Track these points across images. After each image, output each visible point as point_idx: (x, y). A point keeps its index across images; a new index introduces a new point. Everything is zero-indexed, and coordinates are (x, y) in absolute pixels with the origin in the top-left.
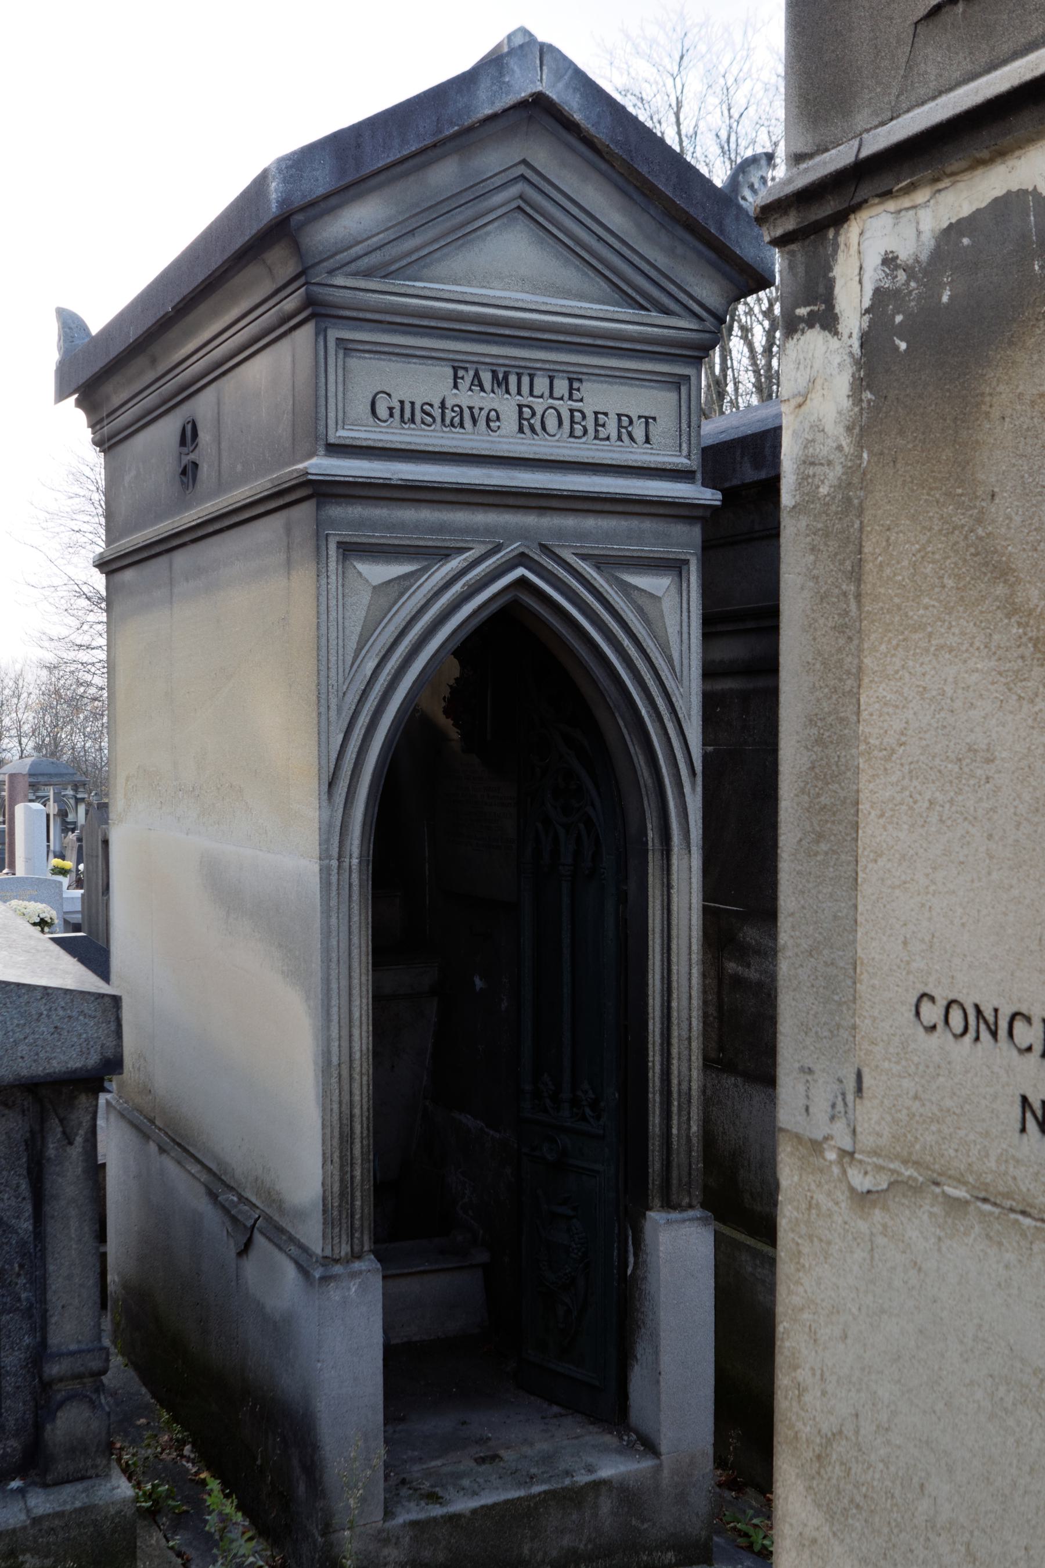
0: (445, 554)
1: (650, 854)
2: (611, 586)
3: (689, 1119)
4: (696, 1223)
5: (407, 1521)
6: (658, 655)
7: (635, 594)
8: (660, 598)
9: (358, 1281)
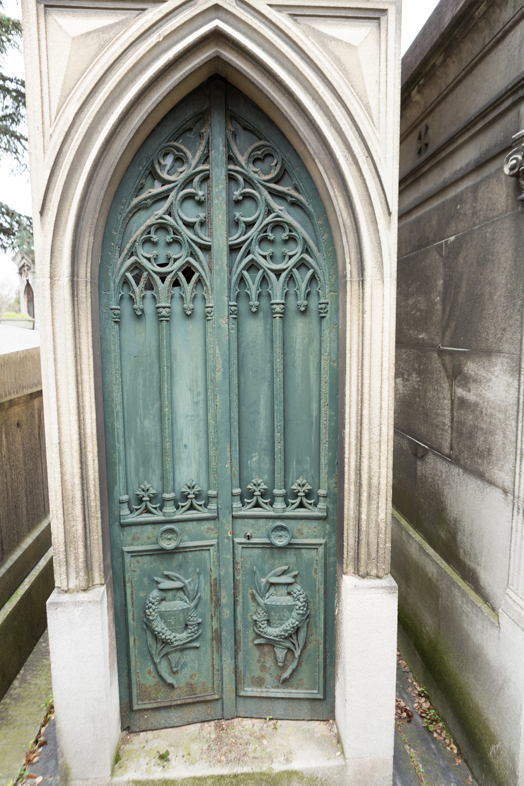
3: (378, 508)
4: (381, 591)
5: (131, 779)
6: (353, 101)
7: (332, 45)
8: (356, 47)
9: (80, 608)
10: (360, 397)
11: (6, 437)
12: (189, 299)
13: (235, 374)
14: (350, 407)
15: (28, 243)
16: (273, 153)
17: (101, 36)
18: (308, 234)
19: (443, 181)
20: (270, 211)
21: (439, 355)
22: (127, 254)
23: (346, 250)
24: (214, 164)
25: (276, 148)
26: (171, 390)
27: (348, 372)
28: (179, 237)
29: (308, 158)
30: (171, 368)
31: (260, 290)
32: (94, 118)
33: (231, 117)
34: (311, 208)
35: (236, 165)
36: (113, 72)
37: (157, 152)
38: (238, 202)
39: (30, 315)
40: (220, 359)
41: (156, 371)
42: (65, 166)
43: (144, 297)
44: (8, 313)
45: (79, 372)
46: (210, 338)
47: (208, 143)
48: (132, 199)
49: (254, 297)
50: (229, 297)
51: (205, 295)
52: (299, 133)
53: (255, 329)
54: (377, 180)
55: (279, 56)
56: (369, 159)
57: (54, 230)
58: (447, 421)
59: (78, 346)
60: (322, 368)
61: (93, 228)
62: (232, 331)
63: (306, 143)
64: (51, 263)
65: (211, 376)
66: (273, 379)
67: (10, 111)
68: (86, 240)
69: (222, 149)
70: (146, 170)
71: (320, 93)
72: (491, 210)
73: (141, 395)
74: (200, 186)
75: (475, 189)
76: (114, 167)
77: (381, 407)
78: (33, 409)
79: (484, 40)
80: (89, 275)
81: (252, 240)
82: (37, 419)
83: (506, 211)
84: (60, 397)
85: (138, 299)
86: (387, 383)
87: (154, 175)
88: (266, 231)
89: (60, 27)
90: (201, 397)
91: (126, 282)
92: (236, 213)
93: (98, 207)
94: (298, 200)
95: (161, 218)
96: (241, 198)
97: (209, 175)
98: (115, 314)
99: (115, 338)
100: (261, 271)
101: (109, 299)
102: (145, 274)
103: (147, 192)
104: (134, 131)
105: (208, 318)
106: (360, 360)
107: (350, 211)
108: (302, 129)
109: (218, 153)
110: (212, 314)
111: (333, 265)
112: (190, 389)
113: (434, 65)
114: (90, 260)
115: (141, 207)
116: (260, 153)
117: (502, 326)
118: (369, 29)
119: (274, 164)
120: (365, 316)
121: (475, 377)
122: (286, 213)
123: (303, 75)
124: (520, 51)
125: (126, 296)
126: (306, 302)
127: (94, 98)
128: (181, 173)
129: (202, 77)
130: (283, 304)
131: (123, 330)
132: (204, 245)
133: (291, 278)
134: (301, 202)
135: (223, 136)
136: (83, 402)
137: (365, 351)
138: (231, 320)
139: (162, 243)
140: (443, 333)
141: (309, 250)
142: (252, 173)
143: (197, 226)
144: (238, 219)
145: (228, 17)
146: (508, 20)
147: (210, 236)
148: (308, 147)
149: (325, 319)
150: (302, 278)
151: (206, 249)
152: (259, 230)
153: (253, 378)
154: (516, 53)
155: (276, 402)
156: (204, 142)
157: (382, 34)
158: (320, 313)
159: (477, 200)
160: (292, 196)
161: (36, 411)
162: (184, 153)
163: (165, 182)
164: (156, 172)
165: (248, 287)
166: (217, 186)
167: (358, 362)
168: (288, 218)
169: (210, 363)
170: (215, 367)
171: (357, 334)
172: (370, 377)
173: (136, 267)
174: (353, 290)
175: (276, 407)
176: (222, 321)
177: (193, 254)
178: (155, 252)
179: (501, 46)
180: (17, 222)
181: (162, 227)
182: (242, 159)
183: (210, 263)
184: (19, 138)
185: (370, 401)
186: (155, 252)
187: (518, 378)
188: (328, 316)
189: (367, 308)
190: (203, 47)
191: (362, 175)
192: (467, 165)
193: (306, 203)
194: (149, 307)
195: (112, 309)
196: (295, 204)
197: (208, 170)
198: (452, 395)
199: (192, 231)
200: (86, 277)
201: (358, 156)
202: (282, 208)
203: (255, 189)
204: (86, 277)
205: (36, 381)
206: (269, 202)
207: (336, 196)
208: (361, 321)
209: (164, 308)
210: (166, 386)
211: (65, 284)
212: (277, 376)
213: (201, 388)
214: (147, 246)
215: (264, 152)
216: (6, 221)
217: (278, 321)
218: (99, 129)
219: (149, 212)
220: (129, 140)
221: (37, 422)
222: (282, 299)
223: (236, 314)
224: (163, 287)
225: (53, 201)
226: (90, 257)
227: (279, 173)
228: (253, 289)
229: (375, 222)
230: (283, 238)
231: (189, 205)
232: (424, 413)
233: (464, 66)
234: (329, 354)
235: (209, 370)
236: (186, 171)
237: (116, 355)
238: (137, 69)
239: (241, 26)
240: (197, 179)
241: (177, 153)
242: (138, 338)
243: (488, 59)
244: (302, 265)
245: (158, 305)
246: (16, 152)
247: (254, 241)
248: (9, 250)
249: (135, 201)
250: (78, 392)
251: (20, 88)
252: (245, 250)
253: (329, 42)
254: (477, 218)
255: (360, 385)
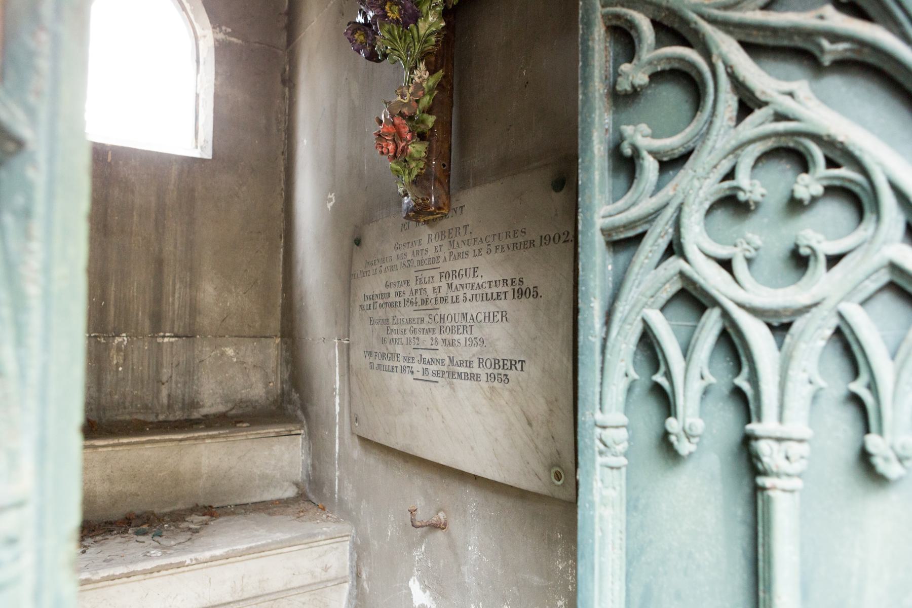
203: (686, 43)
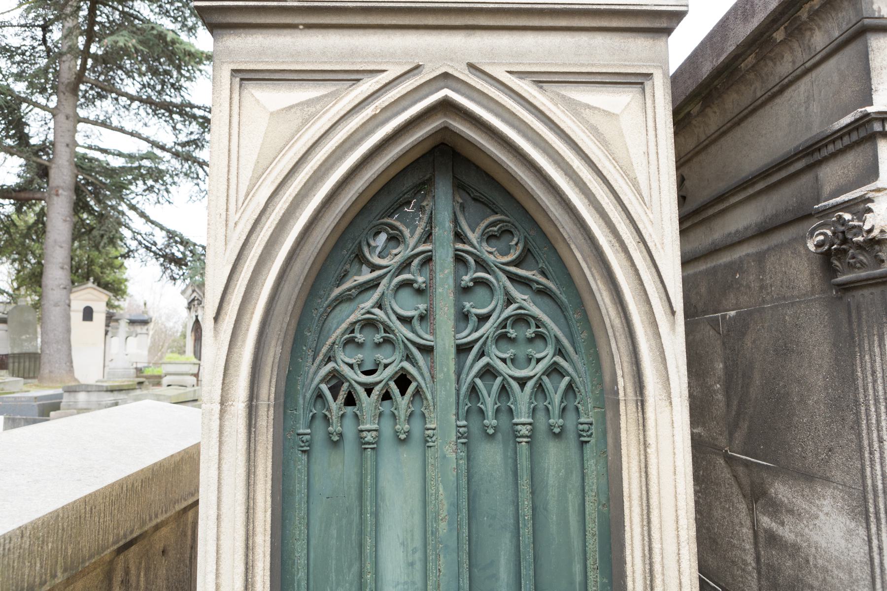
0: (353, 77)
1: (622, 405)
2: (556, 105)
6: (617, 176)
7: (587, 113)
8: (617, 115)
10: (648, 567)
11: (145, 575)
12: (403, 418)
13: (465, 522)
14: (634, 581)
15: (201, 274)
16: (512, 230)
17: (306, 109)
18: (561, 329)
19: (713, 243)
20: (510, 301)
21: (726, 462)
22: (323, 360)
23: (617, 359)
24: (437, 244)
25: (517, 224)
26: (376, 546)
27: (627, 528)
28: (391, 336)
29: (560, 240)
30: (376, 515)
31: (499, 404)
32: (292, 203)
33: (459, 186)
34: (563, 298)
35: (464, 243)
36: (317, 149)
37: (365, 232)
38: (466, 290)
39: (196, 357)
40: (445, 502)
41: (356, 518)
42: (251, 260)
43: (343, 416)
44: (171, 355)
45: (251, 533)
46: (430, 473)
47: (431, 218)
48: (331, 290)
49: (490, 414)
50: (457, 414)
51: (426, 412)
52: (549, 213)
53: (492, 457)
54: (654, 270)
55: (522, 127)
56: (641, 245)
57: (231, 341)
58: (750, 559)
59: (251, 496)
60: (587, 513)
61: (282, 335)
62: (461, 462)
63: (558, 225)
64: (223, 383)
65: (432, 527)
66: (518, 529)
67: (193, 137)
68: (272, 350)
69: (449, 225)
70: (352, 253)
71: (575, 167)
72: (788, 287)
73: (333, 553)
74: (420, 270)
75: (760, 258)
76: (312, 259)
77: (680, 583)
78: (186, 525)
79: (755, 92)
80: (272, 396)
81: (487, 338)
82: (189, 537)
83: (813, 293)
84: (221, 571)
85: (334, 419)
86: (687, 548)
87: (361, 259)
88: (505, 327)
89: (258, 101)
90: (418, 555)
91: (320, 396)
92: (465, 303)
93: (290, 308)
94: (546, 287)
95: (369, 312)
96: (471, 284)
97: (431, 256)
98: (303, 442)
99: (301, 473)
100: (499, 380)
101: (296, 419)
102: (346, 385)
103: (352, 280)
104: (341, 215)
105: (428, 444)
106: (645, 512)
107: (620, 309)
108: (552, 209)
109: (444, 230)
110: (434, 439)
111: (597, 372)
112: (403, 544)
113: (689, 113)
114: (275, 377)
115: (343, 299)
116: (495, 229)
117: (826, 442)
118: (631, 95)
119: (513, 243)
120: (648, 450)
121: (790, 507)
122: (532, 304)
123: (553, 148)
124: (807, 108)
125: (319, 415)
126: (561, 420)
127: (293, 179)
128: (396, 255)
129: (427, 146)
130: (530, 424)
131: (313, 460)
132: (424, 346)
133: (540, 388)
134: (550, 290)
135: (450, 210)
136: (253, 576)
137: (652, 501)
138: (460, 446)
139: (369, 344)
140: (731, 435)
141: (564, 352)
142: (486, 254)
143: (415, 322)
144: (468, 311)
145: (459, 86)
146: (786, 75)
147: (433, 333)
148: (561, 230)
149: (588, 445)
150: (556, 390)
151: (427, 350)
152: (496, 325)
153: (490, 526)
154: (803, 109)
155: (523, 564)
156: (426, 218)
157: (647, 100)
158: (581, 436)
159: (765, 272)
160: (538, 283)
161: (190, 526)
162: (400, 231)
163: (374, 267)
164: (364, 256)
165: (481, 400)
166: (442, 270)
167: (642, 515)
168: (535, 310)
169: (430, 508)
170: (437, 514)
171: (637, 474)
172: (661, 539)
173: (334, 376)
174: (629, 412)
175: (523, 572)
176: (448, 449)
177: (409, 358)
178: (360, 356)
179: (778, 101)
180: (191, 251)
181: (370, 324)
182: (473, 237)
183: (431, 369)
184: (202, 164)
185: (663, 574)
186: (360, 356)
187: (864, 525)
188: (593, 440)
189: (651, 440)
190: (429, 118)
191: (633, 264)
192: (746, 229)
193: (558, 292)
194: (349, 429)
195: (299, 435)
196: (543, 292)
197: (431, 251)
198: (753, 523)
199: (408, 326)
200: (269, 399)
201: (626, 241)
202: (526, 297)
204: (269, 399)
205: (192, 489)
206: (509, 290)
207: (599, 290)
208: (642, 457)
209: (369, 431)
210: (369, 541)
211: (240, 412)
212: (525, 525)
213: (418, 543)
214: (350, 348)
215: (500, 228)
216: (179, 251)
217: (524, 448)
218: (297, 214)
219: (353, 305)
220: (333, 225)
221: (189, 542)
222: (528, 417)
223: (466, 438)
224: (367, 402)
225: (231, 304)
226: (275, 373)
227: (521, 254)
228: (489, 403)
229: (654, 324)
230: (528, 335)
231: (405, 293)
232: (710, 538)
233: (729, 118)
234: (597, 494)
235: (430, 517)
236: (401, 253)
237: (301, 498)
238: (348, 145)
239: (475, 95)
240: (416, 262)
241: (391, 232)
242: (334, 471)
243: (761, 112)
244: (554, 370)
245: (361, 427)
246: (198, 178)
247: (490, 339)
248: (179, 282)
249: (337, 291)
250: (247, 564)
251: (207, 114)
252: (478, 352)
253: (583, 111)
254: (768, 294)
255: (647, 548)
